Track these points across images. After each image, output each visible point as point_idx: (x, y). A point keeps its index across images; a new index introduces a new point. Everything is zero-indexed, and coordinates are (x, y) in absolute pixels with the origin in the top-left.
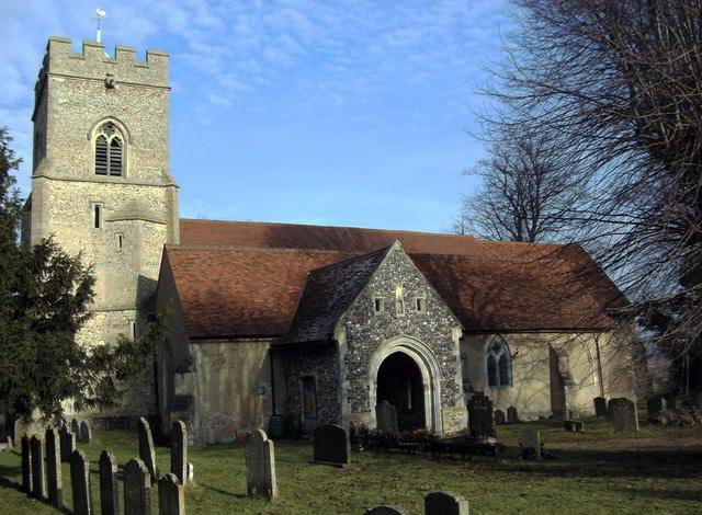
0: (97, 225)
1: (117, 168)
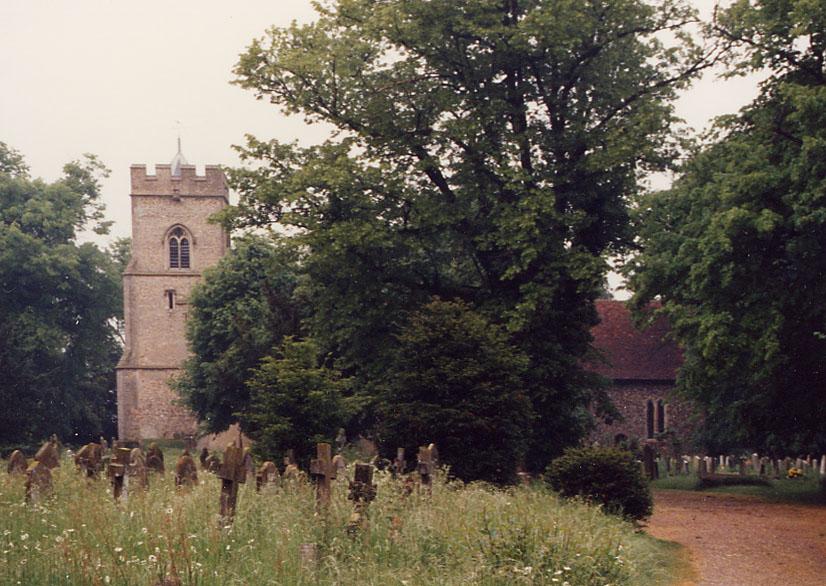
0: (171, 307)
1: (186, 262)
